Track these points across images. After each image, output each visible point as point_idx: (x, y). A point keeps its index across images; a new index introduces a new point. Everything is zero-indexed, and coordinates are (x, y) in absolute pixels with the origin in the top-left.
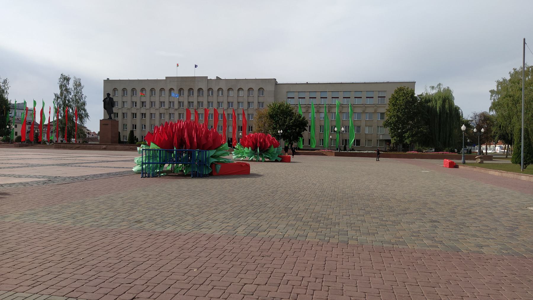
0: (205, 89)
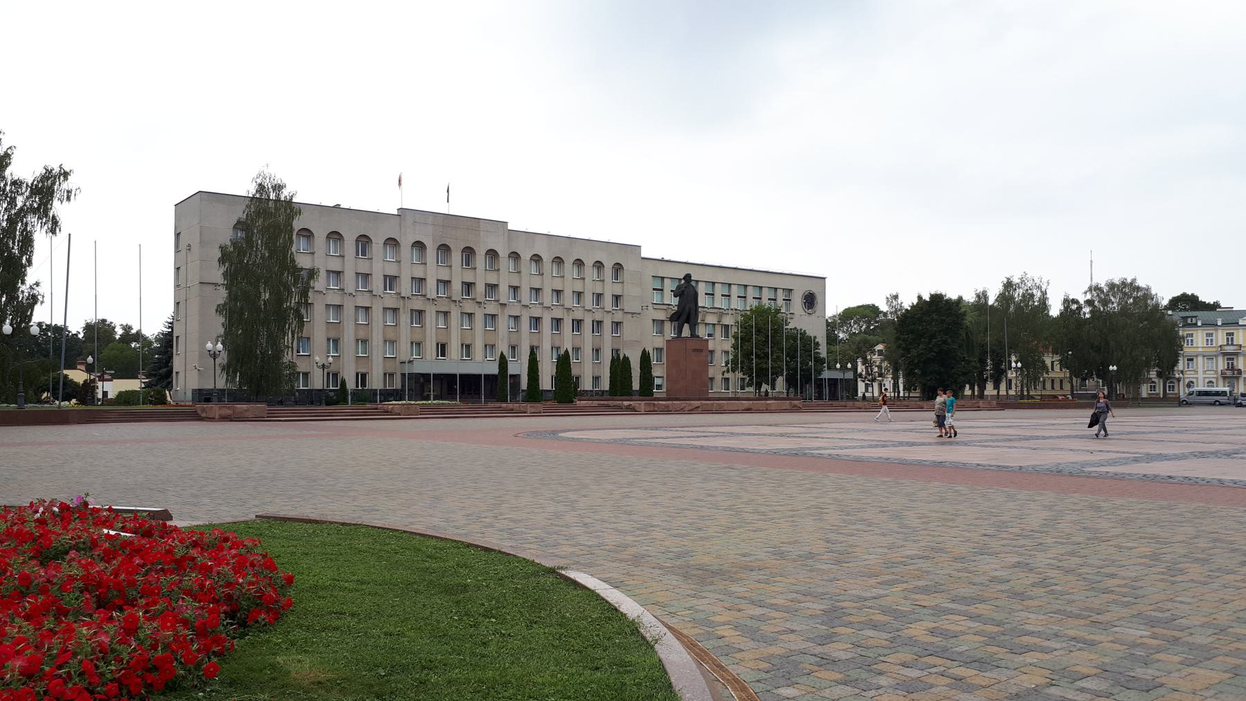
0: (503, 253)
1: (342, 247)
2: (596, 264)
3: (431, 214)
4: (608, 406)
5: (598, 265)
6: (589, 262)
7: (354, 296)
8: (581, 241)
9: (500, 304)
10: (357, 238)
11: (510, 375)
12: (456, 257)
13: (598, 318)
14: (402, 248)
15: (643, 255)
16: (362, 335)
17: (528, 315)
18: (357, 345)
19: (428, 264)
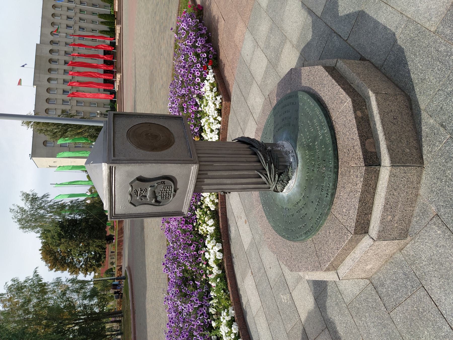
1: (52, 109)
2: (48, 91)
3: (35, 70)
4: (120, 34)
5: (53, 24)
6: (53, 11)
7: (72, 106)
8: (36, 67)
9: (73, 51)
10: (45, 146)
11: (143, 219)
12: (54, 66)
13: (78, 11)
14: (51, 87)
15: (39, 43)
16: (88, 104)
17: (78, 31)
18: (81, 22)
19: (57, 77)
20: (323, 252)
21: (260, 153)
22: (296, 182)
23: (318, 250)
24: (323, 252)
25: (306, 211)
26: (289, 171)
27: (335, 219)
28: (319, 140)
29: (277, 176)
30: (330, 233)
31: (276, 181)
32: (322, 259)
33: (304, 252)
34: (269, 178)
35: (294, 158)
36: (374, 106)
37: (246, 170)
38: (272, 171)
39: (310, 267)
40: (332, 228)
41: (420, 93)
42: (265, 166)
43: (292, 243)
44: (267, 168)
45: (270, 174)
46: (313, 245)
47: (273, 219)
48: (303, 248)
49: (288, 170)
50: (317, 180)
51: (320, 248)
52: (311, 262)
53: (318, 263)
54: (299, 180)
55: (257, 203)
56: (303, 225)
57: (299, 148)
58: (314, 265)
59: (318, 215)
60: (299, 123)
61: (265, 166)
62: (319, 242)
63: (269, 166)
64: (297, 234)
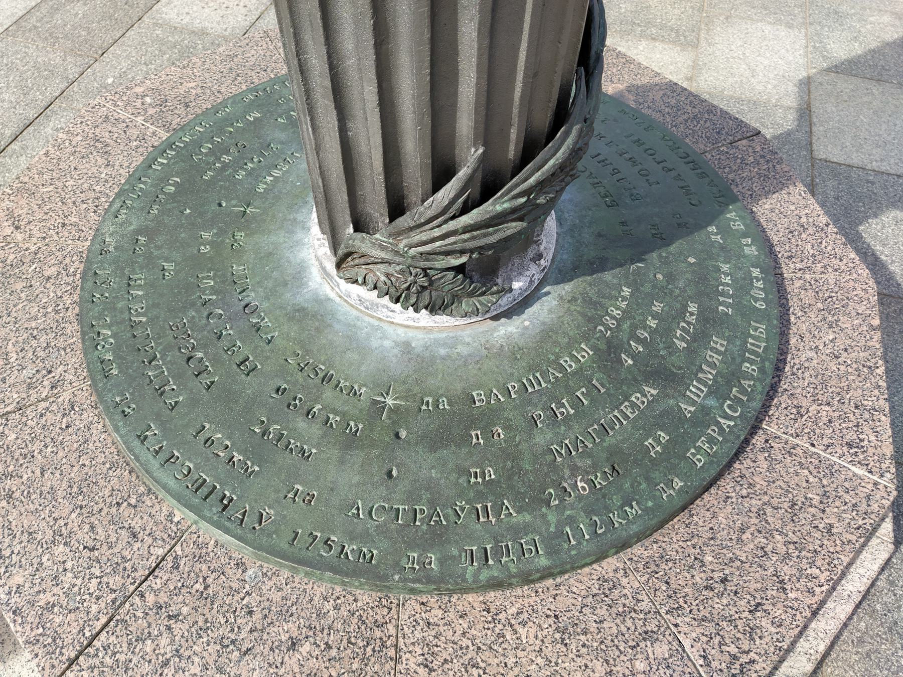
20: (164, 641)
21: (570, 141)
22: (420, 335)
23: (150, 599)
24: (164, 641)
25: (318, 446)
26: (474, 300)
27: (383, 645)
28: (671, 402)
29: (457, 262)
30: (294, 645)
31: (429, 260)
32: (122, 657)
33: (80, 499)
34: (446, 228)
35: (529, 286)
36: (862, 571)
37: (488, 108)
38: (485, 235)
39: (18, 579)
40: (328, 647)
41: (861, 641)
42: (510, 190)
43: (85, 397)
44: (499, 208)
45: (467, 229)
46: (160, 552)
47: (139, 232)
48: (102, 483)
49: (483, 294)
50: (509, 464)
51: (173, 610)
52: (56, 580)
53: (82, 630)
54: (443, 352)
55: (148, 100)
56: (237, 457)
57: (574, 299)
58: (49, 607)
59: (352, 539)
60: (654, 255)
61: (510, 190)
62: (199, 587)
63: (514, 211)
64: (163, 426)
